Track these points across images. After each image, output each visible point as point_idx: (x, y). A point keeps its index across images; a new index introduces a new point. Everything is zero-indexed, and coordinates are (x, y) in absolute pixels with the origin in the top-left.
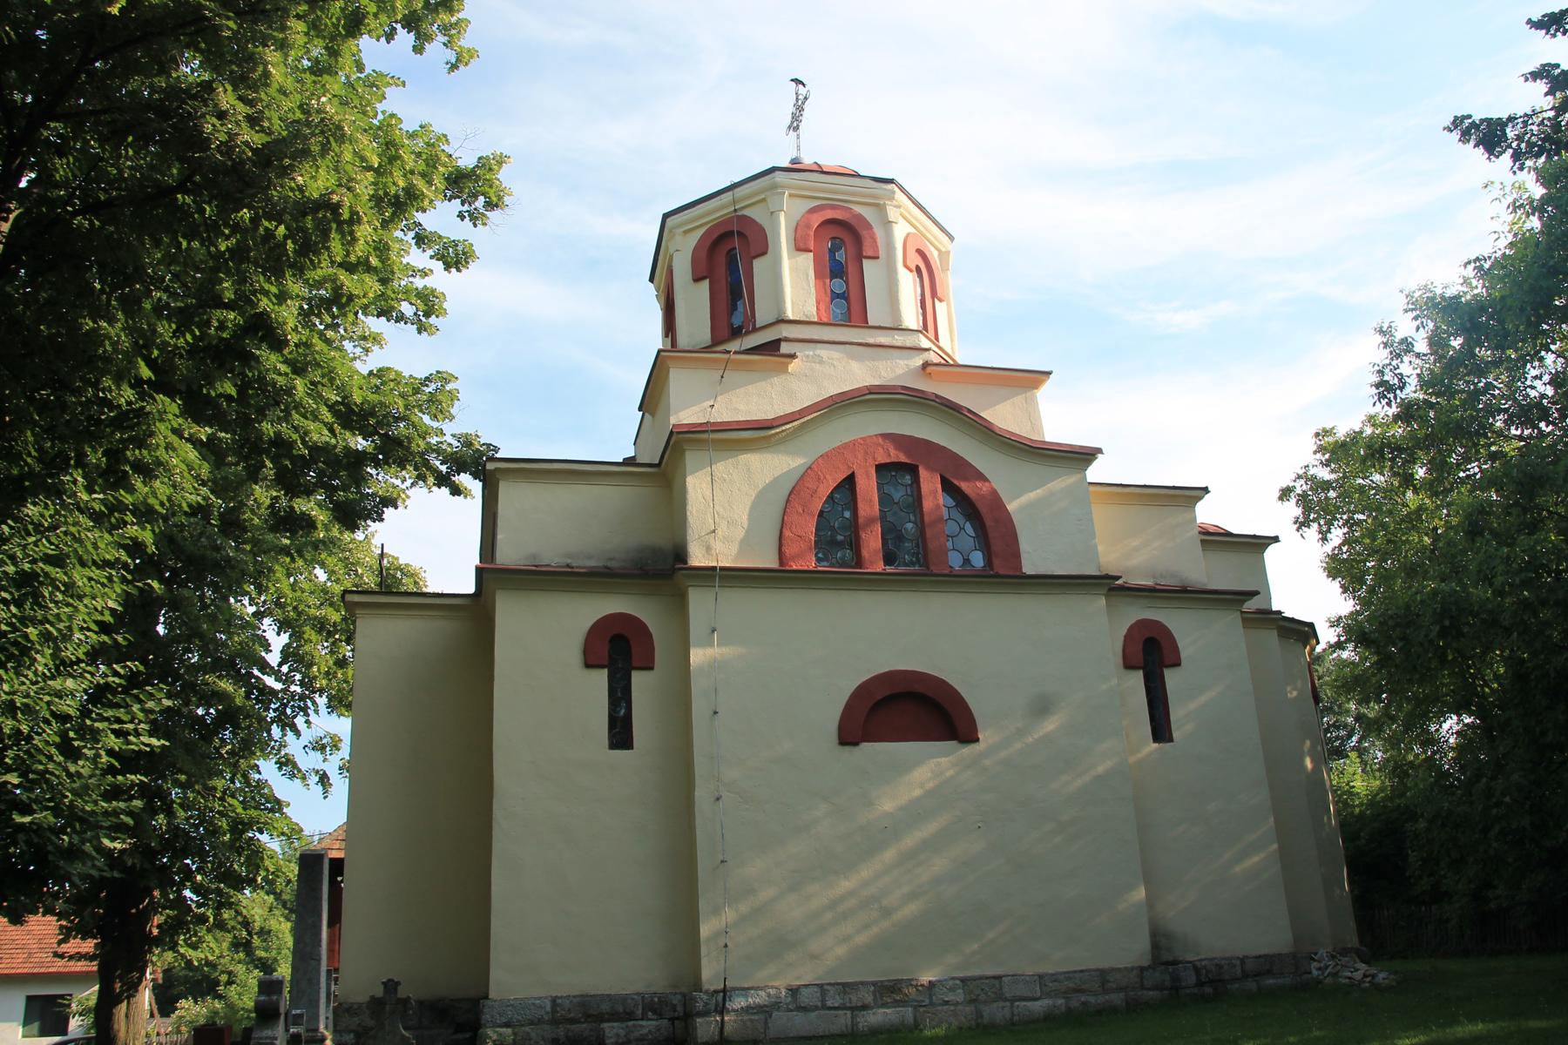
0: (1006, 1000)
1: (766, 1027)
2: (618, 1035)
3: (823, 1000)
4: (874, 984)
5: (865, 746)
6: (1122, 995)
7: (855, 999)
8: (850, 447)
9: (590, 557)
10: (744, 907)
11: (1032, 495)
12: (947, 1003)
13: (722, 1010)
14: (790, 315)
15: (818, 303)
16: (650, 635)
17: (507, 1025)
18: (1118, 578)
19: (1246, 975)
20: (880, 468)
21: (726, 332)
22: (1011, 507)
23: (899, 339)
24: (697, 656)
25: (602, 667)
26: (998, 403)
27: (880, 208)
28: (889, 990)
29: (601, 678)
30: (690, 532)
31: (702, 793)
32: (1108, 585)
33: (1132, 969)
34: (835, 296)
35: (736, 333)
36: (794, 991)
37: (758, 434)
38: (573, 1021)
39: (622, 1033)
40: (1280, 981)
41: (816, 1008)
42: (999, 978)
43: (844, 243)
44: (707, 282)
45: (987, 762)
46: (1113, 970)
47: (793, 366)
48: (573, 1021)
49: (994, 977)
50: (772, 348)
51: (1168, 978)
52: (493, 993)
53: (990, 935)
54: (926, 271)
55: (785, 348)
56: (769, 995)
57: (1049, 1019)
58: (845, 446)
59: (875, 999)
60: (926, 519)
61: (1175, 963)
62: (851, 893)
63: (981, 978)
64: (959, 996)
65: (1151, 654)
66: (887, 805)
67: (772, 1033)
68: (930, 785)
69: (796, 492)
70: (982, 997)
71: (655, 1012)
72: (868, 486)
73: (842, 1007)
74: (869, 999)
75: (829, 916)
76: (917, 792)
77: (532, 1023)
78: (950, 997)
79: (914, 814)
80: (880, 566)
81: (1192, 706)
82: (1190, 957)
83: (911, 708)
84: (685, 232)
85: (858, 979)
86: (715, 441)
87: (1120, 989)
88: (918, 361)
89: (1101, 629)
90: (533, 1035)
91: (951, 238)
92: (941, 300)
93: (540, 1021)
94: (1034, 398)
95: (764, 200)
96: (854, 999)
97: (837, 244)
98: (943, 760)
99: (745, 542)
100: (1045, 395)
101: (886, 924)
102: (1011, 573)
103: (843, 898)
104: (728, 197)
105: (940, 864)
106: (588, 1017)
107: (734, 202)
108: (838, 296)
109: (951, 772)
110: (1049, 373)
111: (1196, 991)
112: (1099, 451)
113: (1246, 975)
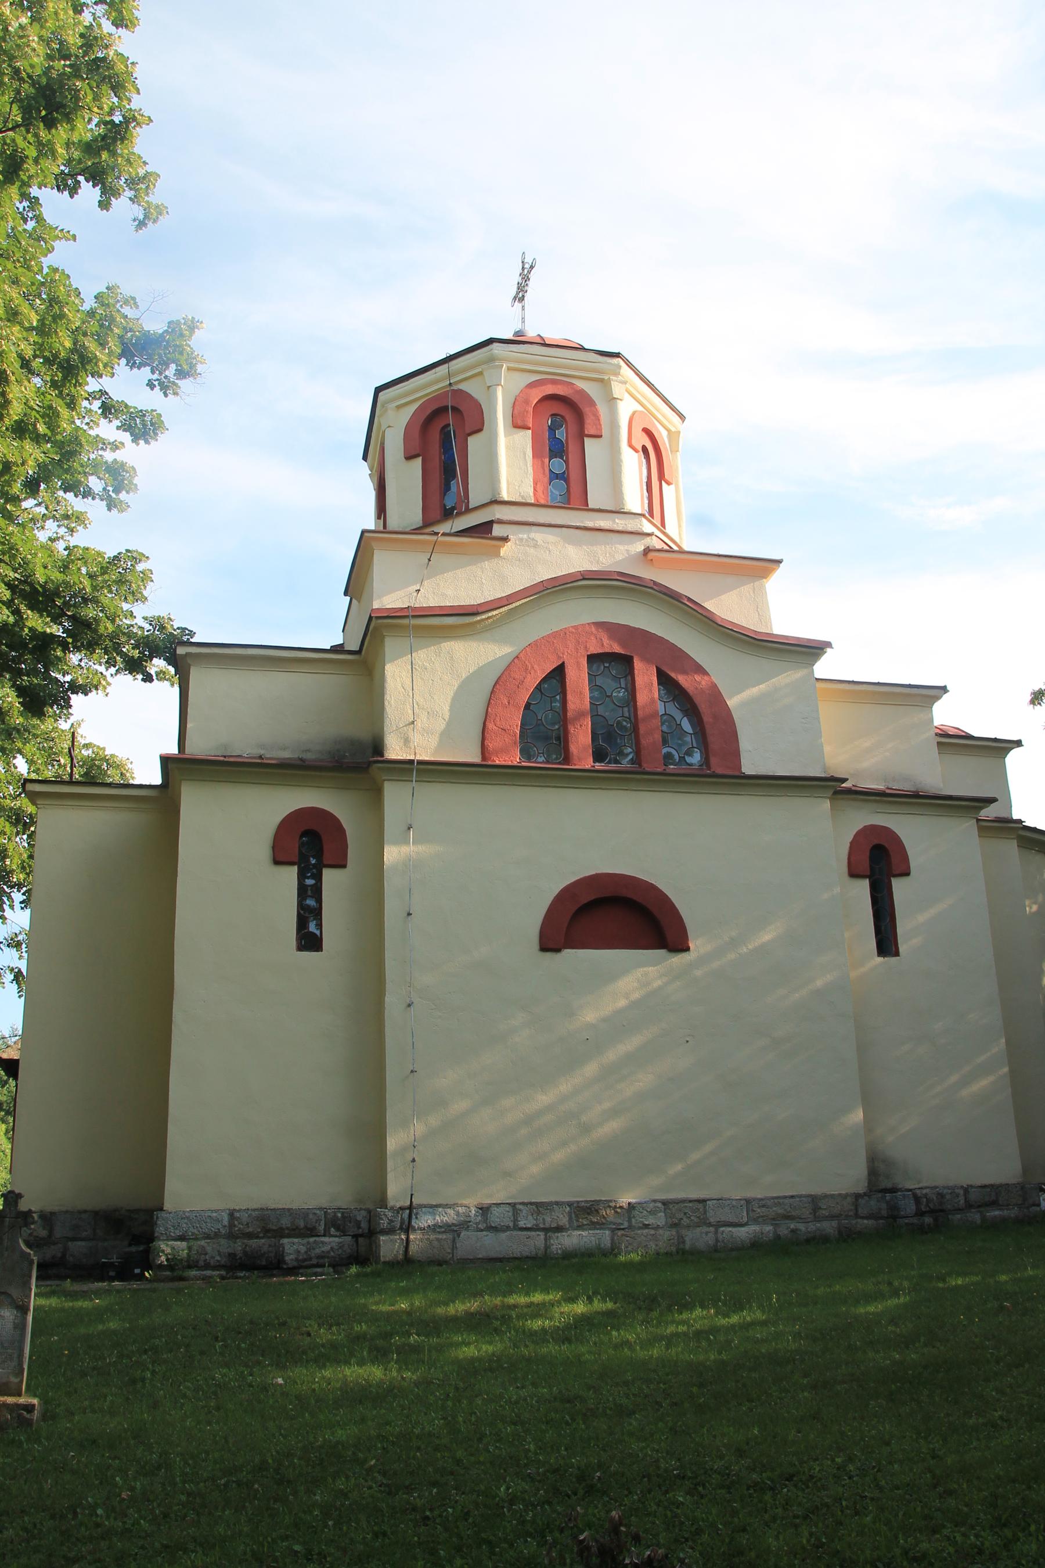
0: (710, 1225)
1: (454, 1247)
3: (515, 1221)
4: (570, 1204)
5: (568, 953)
6: (834, 1223)
7: (548, 1220)
8: (561, 635)
9: (308, 751)
10: (434, 1120)
11: (754, 691)
12: (646, 1226)
13: (407, 1228)
14: (505, 496)
15: (535, 483)
17: (182, 1238)
18: (844, 780)
19: (969, 1206)
20: (592, 658)
21: (437, 513)
22: (731, 703)
23: (620, 523)
24: (392, 854)
25: (291, 863)
27: (604, 384)
28: (586, 1212)
29: (863, 886)
30: (387, 722)
32: (834, 788)
33: (844, 1197)
34: (554, 476)
35: (448, 514)
36: (484, 1210)
37: (463, 620)
38: (250, 1236)
39: (303, 1249)
40: (1006, 1213)
41: (508, 1228)
42: (703, 1201)
43: (565, 420)
45: (698, 973)
46: (825, 1196)
47: (506, 550)
48: (250, 1236)
49: (699, 1201)
50: (483, 530)
52: (167, 1206)
53: (695, 1156)
55: (497, 530)
56: (458, 1214)
57: (755, 1246)
58: (555, 635)
60: (640, 713)
61: (893, 1190)
63: (683, 1201)
64: (660, 1219)
65: (878, 863)
66: (590, 1017)
67: (460, 1253)
68: (636, 996)
69: (502, 683)
71: (338, 1229)
72: (578, 677)
74: (564, 1221)
75: (524, 1131)
76: (622, 1003)
79: (618, 1026)
80: (588, 763)
81: (922, 918)
83: (617, 914)
84: (399, 407)
86: (416, 628)
87: (832, 1217)
88: (639, 547)
89: (826, 835)
90: (209, 1249)
91: (682, 417)
92: (668, 483)
93: (217, 1235)
94: (762, 588)
95: (481, 373)
96: (548, 1219)
97: (557, 422)
99: (445, 735)
100: (774, 585)
104: (442, 370)
105: (644, 1080)
106: (267, 1232)
108: (557, 476)
110: (780, 562)
111: (915, 1220)
112: (829, 645)
113: (969, 1206)
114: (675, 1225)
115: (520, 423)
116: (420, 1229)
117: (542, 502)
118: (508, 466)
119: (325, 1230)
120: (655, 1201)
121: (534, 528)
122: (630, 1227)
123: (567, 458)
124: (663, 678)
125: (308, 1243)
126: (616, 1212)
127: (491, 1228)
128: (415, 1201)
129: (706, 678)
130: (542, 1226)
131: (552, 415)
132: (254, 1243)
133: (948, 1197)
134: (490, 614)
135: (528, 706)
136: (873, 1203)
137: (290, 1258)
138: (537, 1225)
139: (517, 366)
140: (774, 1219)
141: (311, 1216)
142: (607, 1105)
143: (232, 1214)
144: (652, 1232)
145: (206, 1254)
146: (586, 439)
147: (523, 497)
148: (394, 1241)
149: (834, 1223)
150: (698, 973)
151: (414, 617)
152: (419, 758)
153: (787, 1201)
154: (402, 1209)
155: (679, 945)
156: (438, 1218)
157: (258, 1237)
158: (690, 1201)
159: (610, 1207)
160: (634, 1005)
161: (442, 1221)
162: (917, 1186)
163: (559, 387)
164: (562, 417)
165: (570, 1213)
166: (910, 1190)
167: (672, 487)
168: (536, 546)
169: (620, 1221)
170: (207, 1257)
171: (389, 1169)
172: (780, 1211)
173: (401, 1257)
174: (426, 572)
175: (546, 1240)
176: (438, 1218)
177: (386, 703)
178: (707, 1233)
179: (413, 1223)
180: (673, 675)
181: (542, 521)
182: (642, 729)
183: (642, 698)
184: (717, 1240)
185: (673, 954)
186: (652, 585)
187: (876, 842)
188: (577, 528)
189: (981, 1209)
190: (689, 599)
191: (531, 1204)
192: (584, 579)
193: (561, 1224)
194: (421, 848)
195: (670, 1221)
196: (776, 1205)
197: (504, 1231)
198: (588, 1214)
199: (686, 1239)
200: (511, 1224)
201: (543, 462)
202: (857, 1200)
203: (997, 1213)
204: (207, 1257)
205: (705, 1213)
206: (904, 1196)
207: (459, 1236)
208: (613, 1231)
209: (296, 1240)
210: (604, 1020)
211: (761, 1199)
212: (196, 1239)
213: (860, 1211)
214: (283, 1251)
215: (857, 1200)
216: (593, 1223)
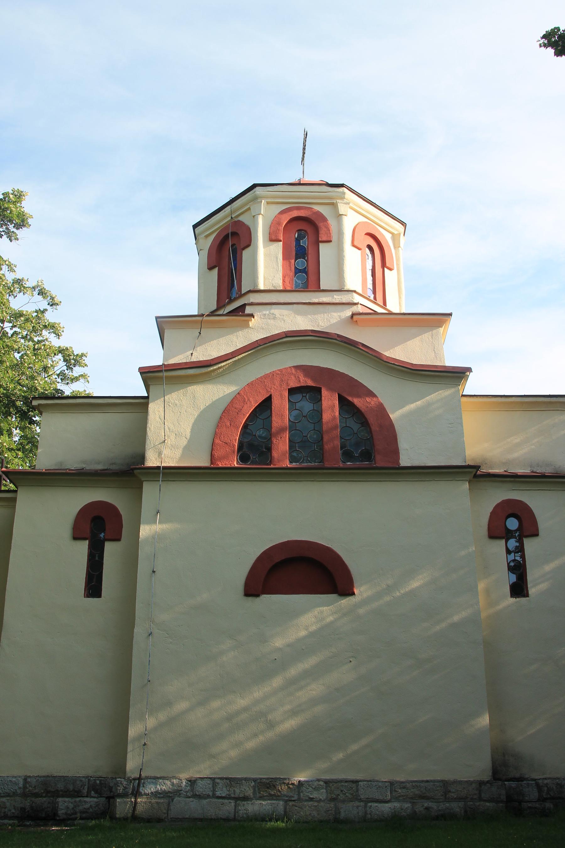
0: (361, 800)
1: (168, 809)
2: (67, 808)
3: (214, 791)
4: (255, 780)
5: (265, 598)
6: (461, 804)
7: (238, 791)
8: (271, 376)
9: (99, 463)
10: (162, 716)
11: (412, 406)
12: (311, 799)
13: (136, 793)
14: (261, 287)
15: (284, 277)
16: (492, 513)
20: (292, 391)
22: (393, 416)
23: (344, 298)
24: (145, 531)
25: (84, 539)
26: (409, 339)
27: (334, 205)
28: (266, 786)
29: (83, 547)
31: (139, 631)
32: (474, 474)
33: (469, 783)
34: (297, 271)
36: (192, 782)
38: (36, 795)
39: (71, 806)
41: (208, 796)
42: (356, 782)
43: (305, 234)
44: (216, 271)
45: (361, 611)
46: (455, 782)
47: (253, 322)
48: (36, 795)
49: (353, 782)
51: (504, 792)
53: (354, 747)
54: (377, 248)
55: (248, 310)
56: (173, 784)
58: (266, 376)
60: (325, 427)
61: (520, 779)
62: (245, 709)
63: (341, 781)
64: (322, 794)
66: (279, 643)
67: (172, 814)
68: (313, 628)
69: (229, 410)
70: (342, 797)
71: (96, 792)
73: (228, 797)
76: (303, 633)
77: (8, 795)
78: (315, 795)
79: (300, 650)
81: (548, 568)
82: (535, 776)
83: (302, 569)
85: (245, 776)
87: (459, 799)
88: (348, 313)
89: (468, 509)
90: (8, 804)
93: (15, 794)
96: (238, 791)
97: (302, 234)
99: (186, 449)
101: (270, 734)
102: (390, 465)
103: (238, 713)
104: (228, 209)
105: (315, 689)
106: (48, 793)
107: (232, 212)
109: (331, 618)
112: (469, 370)
114: (333, 800)
115: (273, 238)
116: (145, 794)
117: (288, 288)
118: (266, 267)
119: (87, 792)
120: (318, 780)
121: (274, 306)
122: (299, 799)
123: (308, 258)
124: (342, 400)
125: (75, 802)
126: (289, 787)
127: (195, 796)
128: (143, 775)
129: (375, 399)
130: (232, 795)
131: (298, 231)
132: (39, 800)
134: (220, 365)
135: (245, 426)
137: (61, 813)
138: (229, 795)
139: (273, 200)
140: (412, 798)
141: (78, 782)
142: (288, 707)
143: (25, 780)
144: (316, 804)
145: (5, 808)
146: (320, 244)
147: (274, 287)
148: (126, 803)
150: (361, 611)
151: (166, 371)
152: (164, 465)
153: (422, 784)
154: (135, 779)
155: (346, 590)
156: (158, 787)
157: (41, 796)
158: (346, 782)
159: (284, 783)
160: (312, 635)
161: (161, 789)
163: (302, 211)
164: (305, 231)
165: (254, 787)
166: (535, 780)
167: (395, 272)
168: (275, 318)
169: (291, 794)
170: (6, 810)
171: (129, 750)
172: (417, 792)
173: (130, 815)
174: (197, 341)
175: (235, 806)
176: (158, 787)
177: (148, 429)
178: (358, 807)
179: (141, 790)
180: (350, 399)
181: (282, 301)
182: (326, 438)
183: (326, 417)
184: (366, 813)
185: (343, 597)
186: (336, 337)
190: (363, 345)
191: (226, 779)
192: (287, 337)
193: (246, 794)
194: (165, 526)
196: (414, 787)
197: (205, 798)
198: (268, 788)
199: (342, 811)
200: (211, 794)
201: (290, 262)
202: (480, 786)
204: (6, 810)
205: (357, 790)
207: (173, 801)
208: (286, 802)
209: (67, 799)
210: (288, 645)
211: (402, 782)
213: (483, 795)
214: (58, 807)
215: (480, 786)
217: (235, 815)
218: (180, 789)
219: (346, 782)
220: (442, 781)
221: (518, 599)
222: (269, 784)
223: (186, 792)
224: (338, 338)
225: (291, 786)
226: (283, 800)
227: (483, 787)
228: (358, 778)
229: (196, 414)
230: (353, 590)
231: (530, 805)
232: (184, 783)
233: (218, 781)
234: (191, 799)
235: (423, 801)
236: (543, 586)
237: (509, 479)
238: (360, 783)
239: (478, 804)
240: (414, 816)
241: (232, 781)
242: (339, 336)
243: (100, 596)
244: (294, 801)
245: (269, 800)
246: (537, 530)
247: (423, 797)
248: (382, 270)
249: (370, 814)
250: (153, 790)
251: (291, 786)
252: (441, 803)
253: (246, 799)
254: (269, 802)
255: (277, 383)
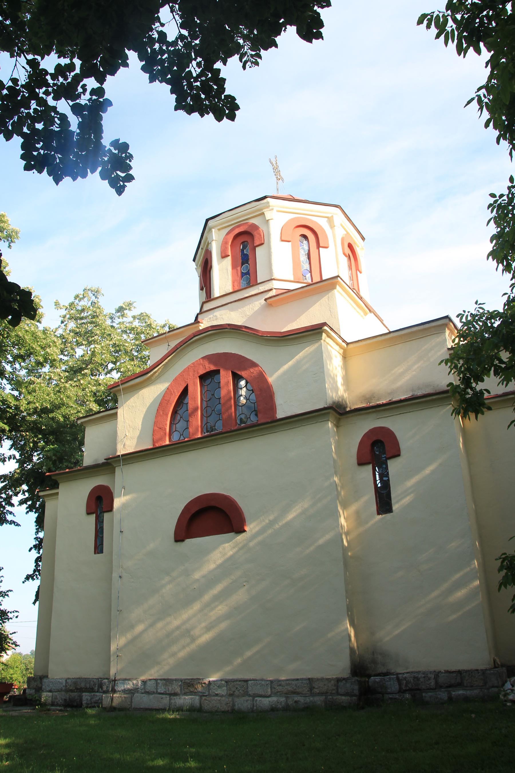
1: (131, 702)
4: (181, 680)
5: (188, 541)
6: (323, 698)
10: (129, 636)
11: (286, 367)
12: (217, 695)
15: (233, 282)
19: (438, 686)
22: (271, 379)
25: (368, 463)
28: (189, 685)
29: (93, 517)
32: (338, 412)
34: (243, 274)
36: (144, 682)
38: (72, 691)
39: (89, 698)
40: (468, 693)
41: (153, 693)
42: (246, 681)
45: (251, 544)
48: (72, 691)
53: (249, 654)
56: (133, 684)
58: (184, 371)
59: (181, 690)
62: (178, 628)
63: (236, 680)
64: (223, 691)
66: (197, 575)
67: (133, 706)
68: (220, 562)
74: (178, 690)
78: (219, 692)
79: (211, 580)
82: (400, 670)
83: (211, 516)
87: (321, 694)
89: (336, 444)
90: (58, 697)
96: (170, 689)
98: (227, 545)
99: (139, 437)
101: (193, 646)
105: (221, 609)
113: (438, 686)
114: (231, 695)
122: (209, 695)
126: (202, 686)
129: (256, 369)
130: (168, 692)
131: (243, 243)
133: (422, 680)
134: (154, 371)
136: (348, 685)
139: (221, 227)
140: (286, 693)
141: (92, 682)
142: (203, 625)
144: (219, 698)
148: (107, 697)
149: (323, 698)
151: (122, 384)
153: (293, 682)
154: (113, 681)
157: (74, 692)
158: (240, 681)
159: (199, 683)
160: (219, 566)
162: (405, 671)
163: (241, 227)
166: (397, 674)
172: (289, 688)
178: (247, 701)
185: (238, 534)
187: (375, 439)
188: (235, 301)
189: (450, 689)
192: (195, 336)
193: (176, 691)
195: (229, 692)
198: (189, 686)
199: (236, 704)
201: (237, 270)
202: (338, 683)
203: (461, 692)
205: (247, 688)
206: (390, 679)
208: (201, 697)
210: (204, 577)
212: (55, 692)
213: (340, 690)
216: (191, 692)
217: (200, 704)
218: (137, 687)
219: (240, 681)
220: (309, 679)
221: (383, 515)
222: (189, 683)
223: (142, 690)
224: (228, 327)
225: (204, 685)
226: (199, 695)
227: (340, 683)
228: (246, 677)
229: (145, 410)
230: (243, 527)
231: (390, 696)
232: (140, 683)
233: (159, 681)
234: (144, 695)
235: (294, 695)
236: (407, 500)
237: (371, 410)
238: (250, 682)
239: (335, 698)
240: (286, 708)
241: (167, 681)
242: (229, 325)
243: (103, 553)
244: (206, 696)
245: (190, 695)
246: (399, 450)
247: (294, 693)
248: (317, 250)
249: (256, 706)
250: (122, 688)
251: (204, 685)
252: (307, 698)
253: (175, 694)
254: (190, 697)
255: (191, 374)
